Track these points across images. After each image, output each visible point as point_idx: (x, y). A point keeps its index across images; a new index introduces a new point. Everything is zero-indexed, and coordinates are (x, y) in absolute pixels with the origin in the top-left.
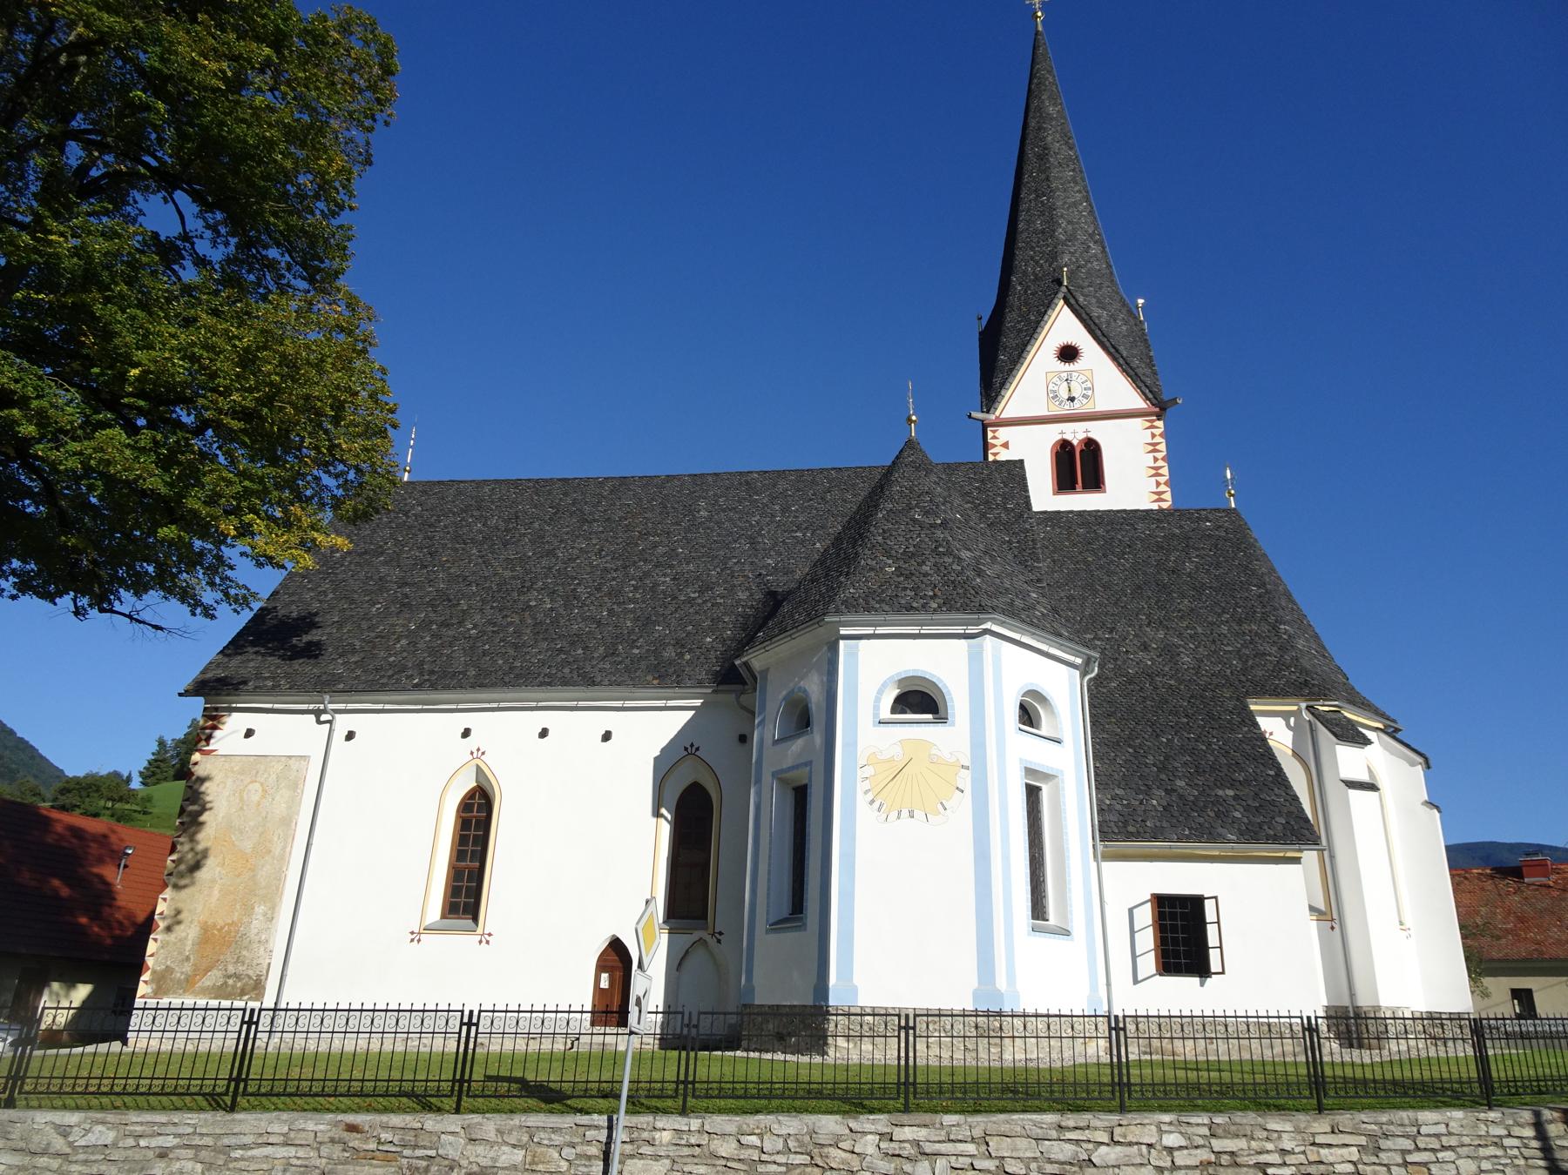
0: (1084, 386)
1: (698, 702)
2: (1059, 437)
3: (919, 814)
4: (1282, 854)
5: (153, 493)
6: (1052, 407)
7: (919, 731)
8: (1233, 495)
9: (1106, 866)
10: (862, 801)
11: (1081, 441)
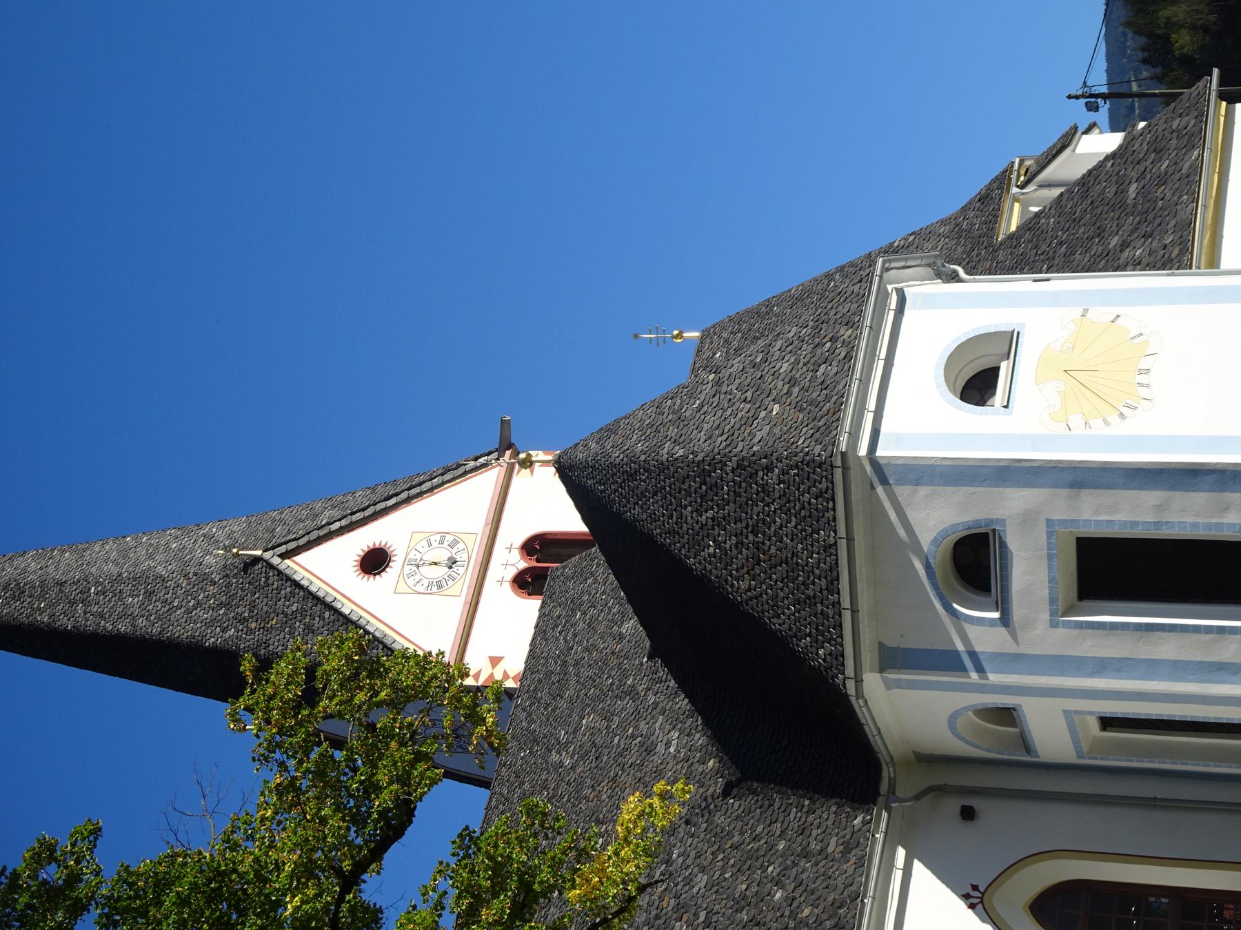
0: (418, 577)
1: (901, 853)
2: (507, 586)
3: (1145, 363)
4: (1222, 119)
6: (455, 590)
8: (681, 333)
9: (1225, 264)
10: (1119, 428)
11: (522, 558)
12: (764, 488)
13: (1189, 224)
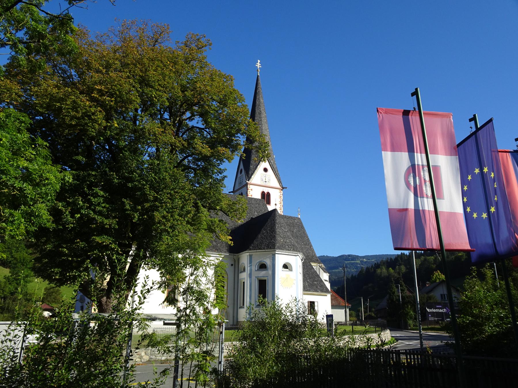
5: (314, 262)
7: (286, 272)
12: (272, 239)
13: (309, 291)
